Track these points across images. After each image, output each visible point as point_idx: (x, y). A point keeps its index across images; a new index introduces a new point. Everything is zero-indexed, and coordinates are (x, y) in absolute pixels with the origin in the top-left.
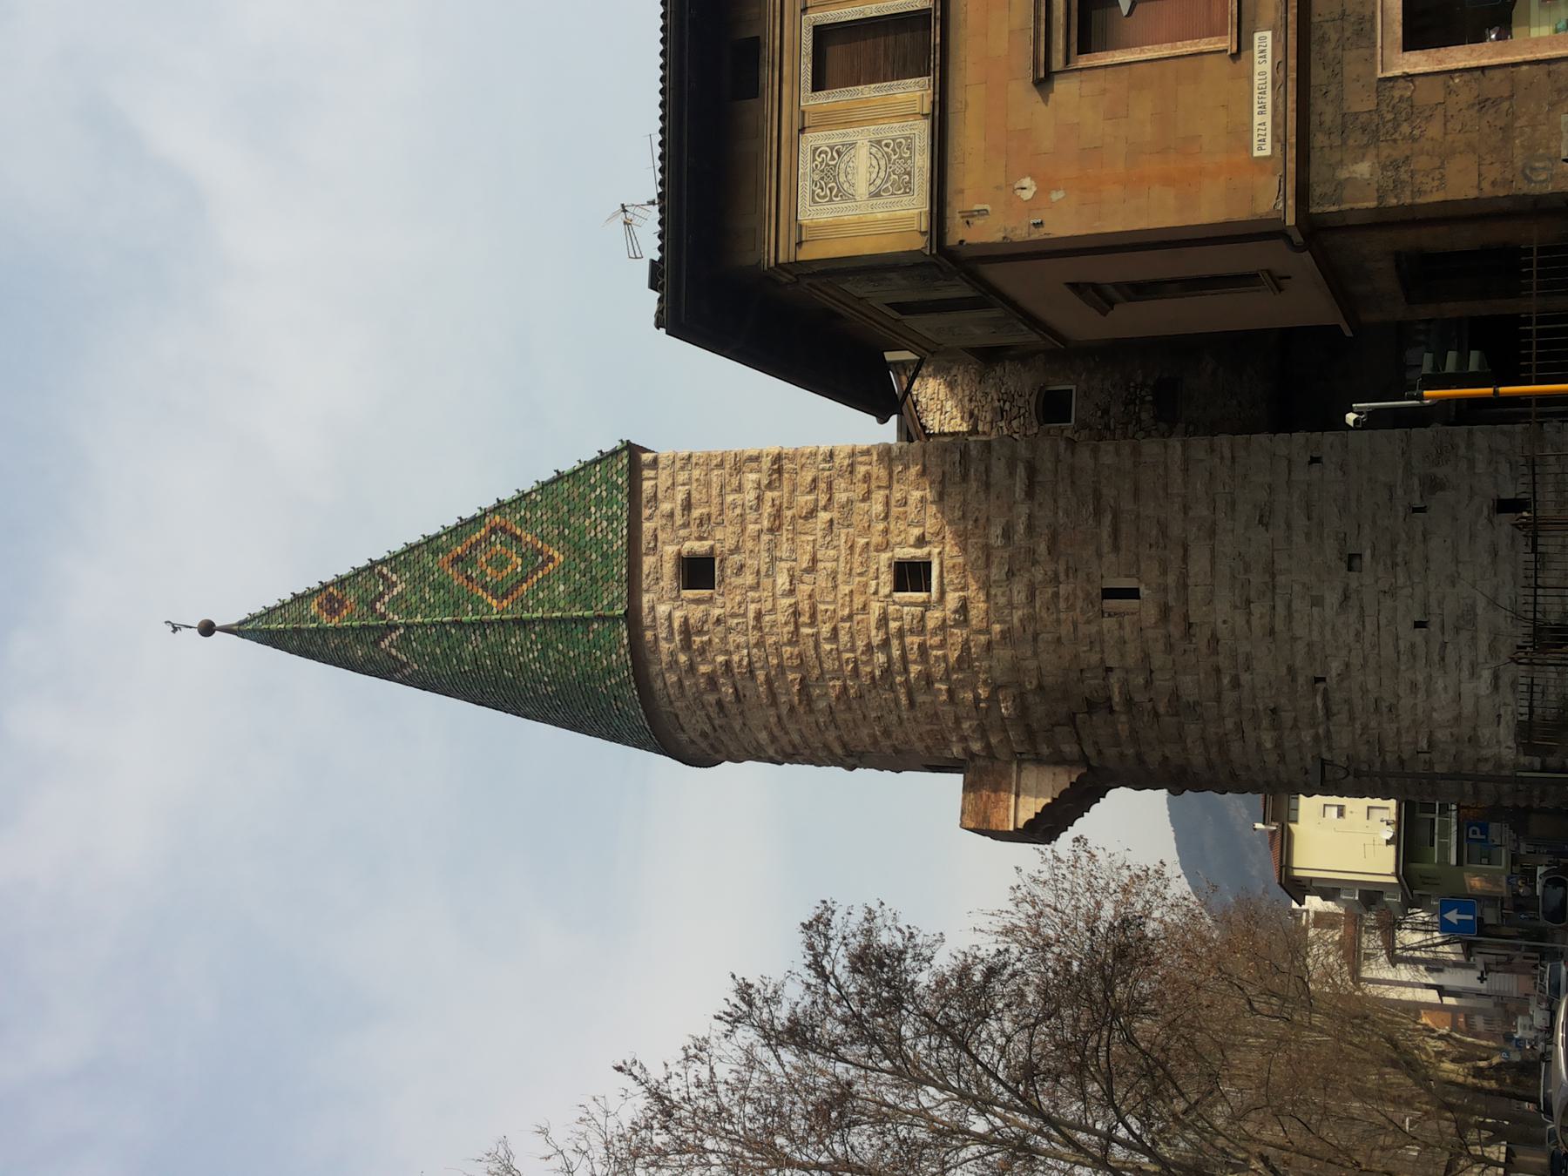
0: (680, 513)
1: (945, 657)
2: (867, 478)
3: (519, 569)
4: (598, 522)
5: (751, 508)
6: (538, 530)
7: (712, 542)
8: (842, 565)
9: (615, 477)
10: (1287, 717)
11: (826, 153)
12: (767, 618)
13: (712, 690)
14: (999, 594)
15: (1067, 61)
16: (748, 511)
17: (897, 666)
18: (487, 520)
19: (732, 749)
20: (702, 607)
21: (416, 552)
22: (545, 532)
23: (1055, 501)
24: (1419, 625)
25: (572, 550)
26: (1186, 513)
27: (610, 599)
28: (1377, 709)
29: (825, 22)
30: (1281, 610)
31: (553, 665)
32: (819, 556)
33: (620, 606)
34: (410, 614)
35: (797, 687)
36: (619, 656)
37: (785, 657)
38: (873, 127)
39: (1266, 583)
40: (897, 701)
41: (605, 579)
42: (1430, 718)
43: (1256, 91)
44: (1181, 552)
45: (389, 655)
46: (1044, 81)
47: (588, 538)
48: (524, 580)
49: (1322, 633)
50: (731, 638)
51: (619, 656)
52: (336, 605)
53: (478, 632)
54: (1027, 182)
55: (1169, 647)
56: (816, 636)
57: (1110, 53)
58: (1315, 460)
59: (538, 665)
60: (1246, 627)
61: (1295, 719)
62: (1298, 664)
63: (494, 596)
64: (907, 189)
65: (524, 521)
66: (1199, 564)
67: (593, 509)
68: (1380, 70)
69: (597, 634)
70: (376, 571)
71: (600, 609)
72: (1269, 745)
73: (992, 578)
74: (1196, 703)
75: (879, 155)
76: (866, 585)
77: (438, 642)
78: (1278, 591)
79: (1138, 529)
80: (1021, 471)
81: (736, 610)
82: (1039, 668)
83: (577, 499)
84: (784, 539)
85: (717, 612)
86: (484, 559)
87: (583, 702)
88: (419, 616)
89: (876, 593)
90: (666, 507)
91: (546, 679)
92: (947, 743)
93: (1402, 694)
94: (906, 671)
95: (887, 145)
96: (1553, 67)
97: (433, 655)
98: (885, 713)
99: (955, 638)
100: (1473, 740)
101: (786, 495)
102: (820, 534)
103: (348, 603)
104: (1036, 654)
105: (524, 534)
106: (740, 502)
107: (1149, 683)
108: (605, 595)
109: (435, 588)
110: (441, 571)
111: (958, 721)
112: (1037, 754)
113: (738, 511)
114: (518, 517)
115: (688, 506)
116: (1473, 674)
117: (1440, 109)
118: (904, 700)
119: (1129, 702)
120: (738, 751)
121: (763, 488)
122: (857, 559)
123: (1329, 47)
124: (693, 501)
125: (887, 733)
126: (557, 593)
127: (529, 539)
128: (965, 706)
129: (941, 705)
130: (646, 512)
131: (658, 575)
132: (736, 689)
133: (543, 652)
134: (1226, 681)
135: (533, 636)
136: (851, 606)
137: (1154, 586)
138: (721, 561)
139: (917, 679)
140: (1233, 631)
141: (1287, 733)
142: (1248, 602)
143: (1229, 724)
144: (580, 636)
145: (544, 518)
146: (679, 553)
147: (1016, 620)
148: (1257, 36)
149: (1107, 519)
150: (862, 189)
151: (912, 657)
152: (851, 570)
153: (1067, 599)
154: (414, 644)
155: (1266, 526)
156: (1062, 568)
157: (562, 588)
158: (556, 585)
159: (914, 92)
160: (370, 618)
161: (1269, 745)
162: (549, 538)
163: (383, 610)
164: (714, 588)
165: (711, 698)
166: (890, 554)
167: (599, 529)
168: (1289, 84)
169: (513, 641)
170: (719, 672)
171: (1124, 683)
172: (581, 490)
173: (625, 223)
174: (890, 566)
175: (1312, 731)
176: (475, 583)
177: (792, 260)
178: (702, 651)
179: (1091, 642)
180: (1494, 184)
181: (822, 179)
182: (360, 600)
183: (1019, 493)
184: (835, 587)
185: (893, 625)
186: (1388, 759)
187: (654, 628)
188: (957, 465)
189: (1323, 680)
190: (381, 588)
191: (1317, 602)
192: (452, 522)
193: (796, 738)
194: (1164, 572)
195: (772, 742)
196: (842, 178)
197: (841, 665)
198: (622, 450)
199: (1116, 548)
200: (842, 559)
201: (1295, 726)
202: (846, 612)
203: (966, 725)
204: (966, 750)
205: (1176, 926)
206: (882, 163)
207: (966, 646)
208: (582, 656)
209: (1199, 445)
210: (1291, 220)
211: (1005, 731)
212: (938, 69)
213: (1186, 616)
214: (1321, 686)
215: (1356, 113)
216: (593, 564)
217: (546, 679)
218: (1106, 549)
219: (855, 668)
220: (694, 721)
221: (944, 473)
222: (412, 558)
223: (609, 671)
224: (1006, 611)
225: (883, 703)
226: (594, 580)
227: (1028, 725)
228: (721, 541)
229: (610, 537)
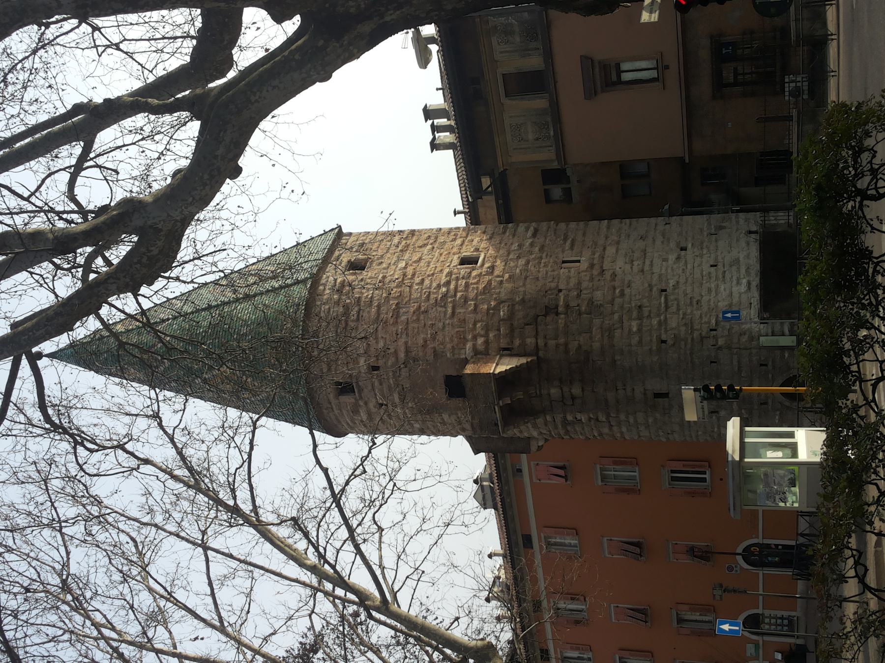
28: (691, 304)
30: (648, 262)
40: (445, 313)
42: (717, 306)
49: (666, 270)
55: (592, 279)
62: (654, 283)
93: (703, 294)
94: (455, 295)
104: (524, 285)
116: (738, 283)
118: (450, 310)
119: (567, 306)
134: (617, 291)
139: (460, 298)
142: (632, 261)
143: (616, 316)
151: (460, 289)
161: (635, 329)
171: (566, 296)
175: (658, 319)
187: (325, 285)
189: (665, 291)
191: (665, 260)
201: (649, 316)
207: (490, 282)
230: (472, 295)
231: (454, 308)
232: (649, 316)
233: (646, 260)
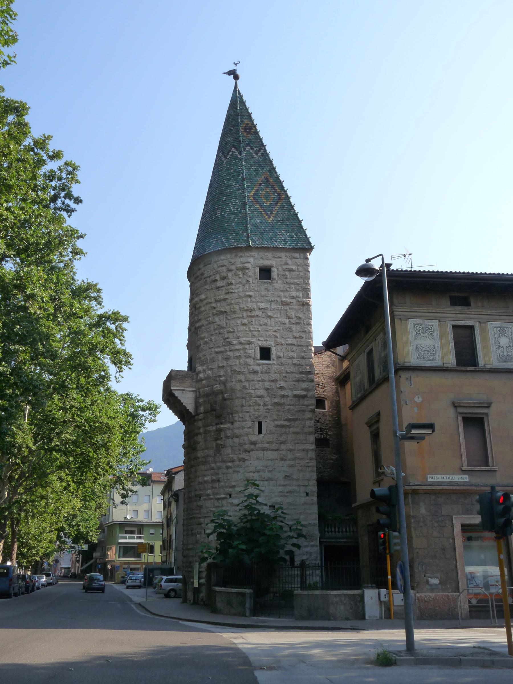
0: (287, 267)
1: (236, 365)
2: (301, 337)
3: (265, 204)
5: (290, 294)
6: (280, 212)
7: (277, 279)
8: (269, 328)
10: (216, 485)
11: (431, 329)
12: (249, 299)
13: (221, 278)
14: (259, 385)
16: (288, 293)
17: (232, 348)
18: (283, 192)
19: (197, 284)
20: (253, 275)
22: (279, 215)
23: (293, 405)
26: (289, 450)
27: (255, 240)
29: (475, 330)
31: (229, 217)
32: (272, 319)
34: (246, 160)
35: (223, 310)
37: (234, 306)
38: (440, 346)
43: (449, 476)
44: (275, 449)
45: (229, 151)
46: (455, 406)
47: (277, 232)
48: (261, 206)
52: (248, 131)
53: (240, 187)
54: (420, 399)
55: (241, 445)
56: (243, 317)
58: (307, 494)
59: (228, 210)
60: (249, 471)
63: (254, 194)
64: (419, 358)
66: (271, 455)
67: (288, 234)
70: (262, 147)
72: (206, 479)
73: (265, 382)
74: (221, 454)
75: (430, 348)
76: (262, 336)
77: (235, 171)
78: (262, 482)
79: (283, 434)
80: (304, 393)
83: (292, 228)
84: (278, 306)
85: (251, 280)
86: (268, 190)
87: (214, 228)
89: (259, 340)
90: (290, 262)
91: (223, 214)
92: (201, 365)
95: (433, 351)
97: (230, 169)
98: (214, 342)
101: (294, 307)
102: (280, 319)
105: (278, 207)
106: (291, 290)
107: (228, 437)
110: (263, 173)
111: (211, 369)
112: (199, 397)
113: (288, 289)
115: (291, 270)
118: (218, 350)
120: (196, 287)
121: (297, 299)
122: (271, 333)
124: (292, 273)
125: (206, 343)
126: (256, 219)
127: (276, 208)
128: (217, 372)
130: (288, 255)
131: (264, 259)
132: (221, 287)
134: (230, 464)
135: (239, 209)
137: (263, 439)
138: (270, 282)
140: (247, 467)
141: (210, 485)
143: (213, 465)
144: (240, 228)
145: (285, 215)
146: (273, 267)
147: (250, 391)
148: (467, 476)
149: (287, 423)
150: (419, 342)
151: (235, 353)
152: (268, 331)
153: (258, 409)
154: (234, 162)
155: (284, 478)
156: (269, 407)
157: (259, 221)
158: (259, 219)
159: (451, 360)
160: (243, 144)
161: (206, 479)
162: (277, 217)
163: (247, 149)
164: (260, 279)
165: (218, 277)
166: (273, 346)
167: (281, 236)
168: (451, 487)
169: (237, 201)
170: (228, 281)
171: (228, 429)
172: (296, 230)
173: (405, 255)
175: (211, 494)
176: (259, 187)
177: (395, 317)
178: (236, 275)
179: (242, 417)
180: (418, 553)
182: (250, 140)
183: (296, 392)
184: (261, 325)
185: (247, 346)
186: (201, 519)
188: (306, 370)
190: (255, 149)
192: (281, 178)
193: (203, 309)
194: (268, 443)
195: (200, 300)
196: (422, 335)
198: (311, 246)
199: (276, 426)
200: (271, 328)
201: (213, 487)
202: (252, 329)
203: (210, 372)
204: (200, 372)
205: (13, 431)
206: (428, 349)
208: (233, 228)
209: (312, 455)
211: (208, 386)
212: (459, 369)
213: (253, 450)
214: (228, 496)
215: (441, 509)
216: (268, 234)
217: (223, 214)
218: (276, 423)
219: (231, 332)
220: (208, 270)
221: (302, 365)
222: (267, 162)
223: (227, 239)
224: (253, 388)
225: (218, 342)
226: (262, 234)
227: (210, 394)
229: (278, 240)
230: (231, 362)
231: (222, 352)
232: (213, 487)
233: (260, 481)
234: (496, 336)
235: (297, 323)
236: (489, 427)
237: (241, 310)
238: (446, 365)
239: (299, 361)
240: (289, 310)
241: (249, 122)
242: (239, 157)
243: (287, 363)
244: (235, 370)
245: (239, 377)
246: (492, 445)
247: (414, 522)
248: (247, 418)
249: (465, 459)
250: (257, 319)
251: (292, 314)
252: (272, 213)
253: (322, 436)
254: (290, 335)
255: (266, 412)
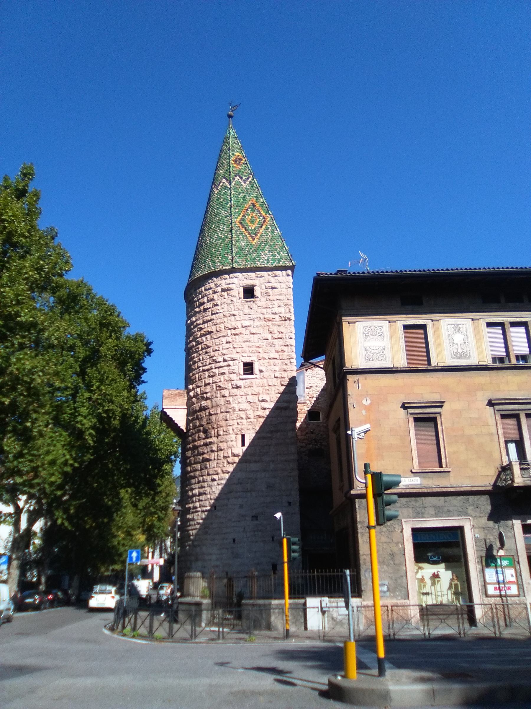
1: (221, 381)
2: (283, 351)
3: (250, 228)
4: (267, 256)
7: (260, 297)
9: (282, 261)
15: (411, 414)
16: (271, 309)
17: (217, 365)
18: (268, 215)
21: (257, 190)
23: (275, 417)
24: (234, 540)
25: (257, 247)
27: (239, 261)
32: (255, 335)
33: (237, 265)
34: (235, 189)
36: (219, 266)
37: (220, 325)
39: (247, 489)
40: (206, 365)
41: (246, 260)
45: (220, 182)
47: (261, 252)
48: (246, 230)
50: (226, 306)
51: (219, 266)
52: (238, 162)
53: (228, 214)
54: (369, 402)
56: (227, 336)
57: (414, 429)
58: (290, 504)
59: (216, 237)
61: (202, 501)
63: (241, 219)
64: (367, 360)
65: (268, 229)
67: (271, 254)
68: (405, 520)
69: (227, 258)
71: (236, 258)
75: (379, 350)
81: (236, 307)
82: (217, 414)
83: (275, 248)
84: (261, 323)
88: (234, 192)
91: (211, 240)
95: (383, 352)
96: (404, 577)
99: (227, 384)
100: (197, 560)
101: (277, 323)
102: (263, 335)
103: (239, 166)
108: (241, 260)
109: (244, 198)
113: (271, 306)
114: (269, 226)
117: (391, 541)
118: (205, 368)
123: (413, 503)
129: (205, 381)
130: (270, 273)
133: (221, 238)
135: (226, 234)
136: (238, 348)
138: (254, 301)
141: (198, 498)
142: (241, 484)
144: (226, 251)
145: (268, 236)
148: (418, 478)
149: (269, 435)
150: (368, 344)
154: (224, 191)
157: (243, 244)
162: (261, 238)
163: (236, 179)
167: (264, 256)
170: (214, 302)
172: (278, 249)
174: (252, 361)
175: (198, 506)
179: (226, 431)
181: (372, 330)
182: (240, 171)
185: (231, 363)
189: (215, 509)
190: (244, 178)
196: (372, 337)
197: (217, 345)
200: (254, 344)
201: (200, 501)
208: (219, 253)
210: (353, 492)
217: (211, 240)
219: (216, 350)
223: (214, 263)
225: (205, 361)
226: (246, 255)
228: (260, 300)
230: (216, 379)
231: (208, 370)
232: (200, 501)
234: (450, 333)
235: (279, 338)
236: (442, 427)
237: (225, 329)
238: (395, 366)
239: (281, 374)
240: (271, 326)
241: (239, 155)
242: (229, 186)
243: (270, 377)
244: (220, 386)
245: (223, 393)
246: (446, 445)
247: (361, 527)
248: (231, 432)
249: (416, 461)
250: (241, 336)
251: (275, 329)
252: (256, 235)
253: (317, 447)
254: (273, 349)
255: (249, 425)
